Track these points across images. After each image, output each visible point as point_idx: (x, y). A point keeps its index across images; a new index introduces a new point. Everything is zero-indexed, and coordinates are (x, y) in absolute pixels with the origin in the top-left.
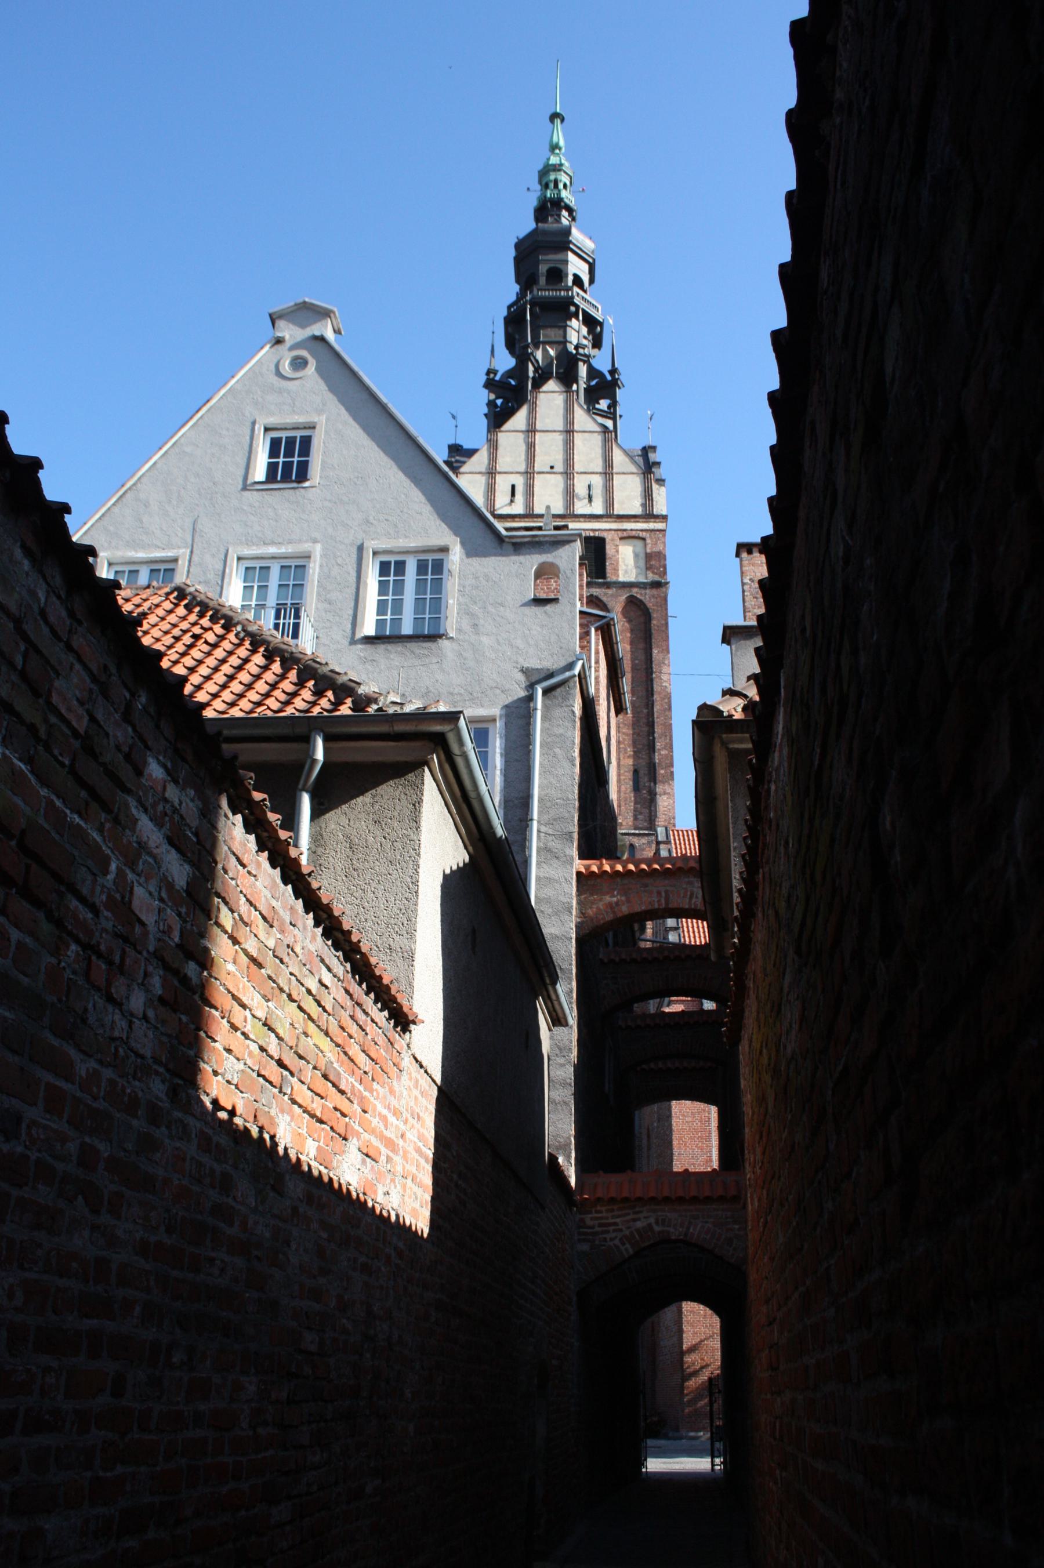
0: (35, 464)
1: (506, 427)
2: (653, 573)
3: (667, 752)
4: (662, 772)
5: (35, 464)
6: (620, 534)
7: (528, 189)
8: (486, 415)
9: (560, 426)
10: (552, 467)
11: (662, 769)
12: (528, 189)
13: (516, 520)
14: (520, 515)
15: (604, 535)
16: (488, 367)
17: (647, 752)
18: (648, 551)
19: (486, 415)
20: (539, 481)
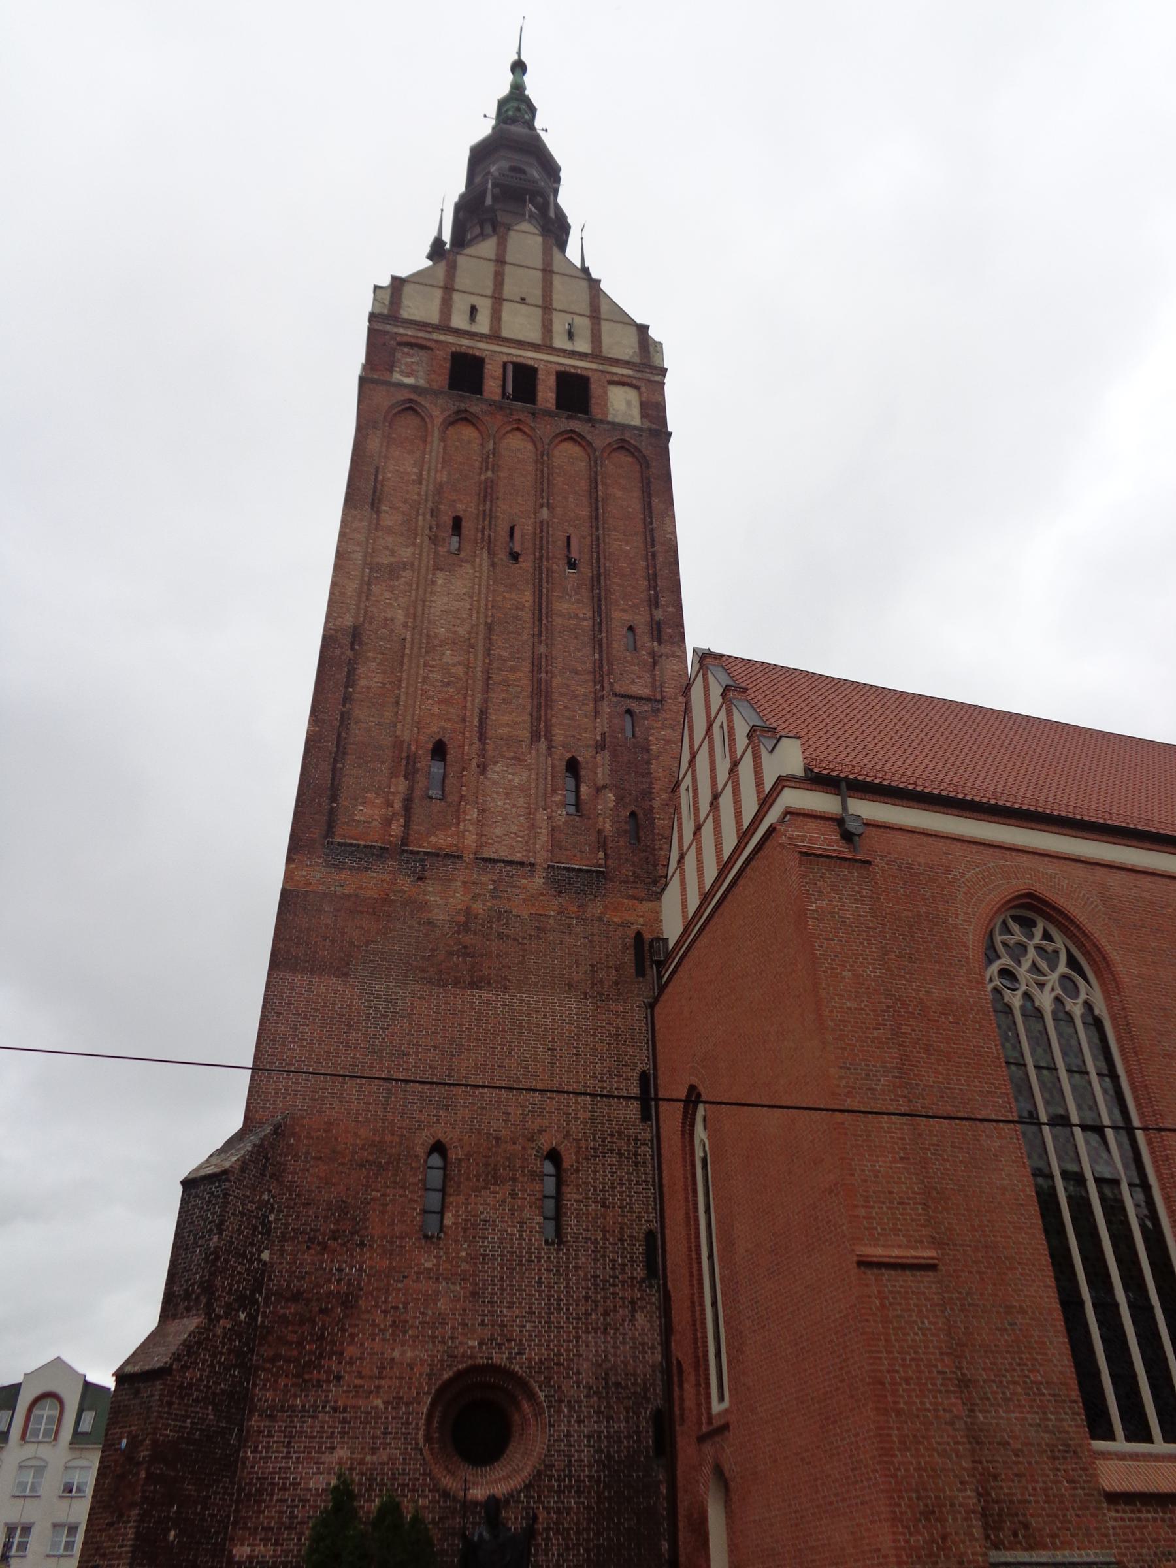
0: (599, 281)
1: (468, 251)
2: (650, 422)
3: (674, 610)
4: (669, 631)
5: (599, 281)
6: (609, 377)
7: (485, 116)
8: (377, 288)
9: (539, 265)
10: (523, 299)
11: (669, 628)
12: (485, 116)
13: (476, 338)
14: (482, 334)
15: (590, 374)
16: (516, 57)
17: (647, 608)
18: (644, 399)
19: (377, 288)
20: (507, 309)
